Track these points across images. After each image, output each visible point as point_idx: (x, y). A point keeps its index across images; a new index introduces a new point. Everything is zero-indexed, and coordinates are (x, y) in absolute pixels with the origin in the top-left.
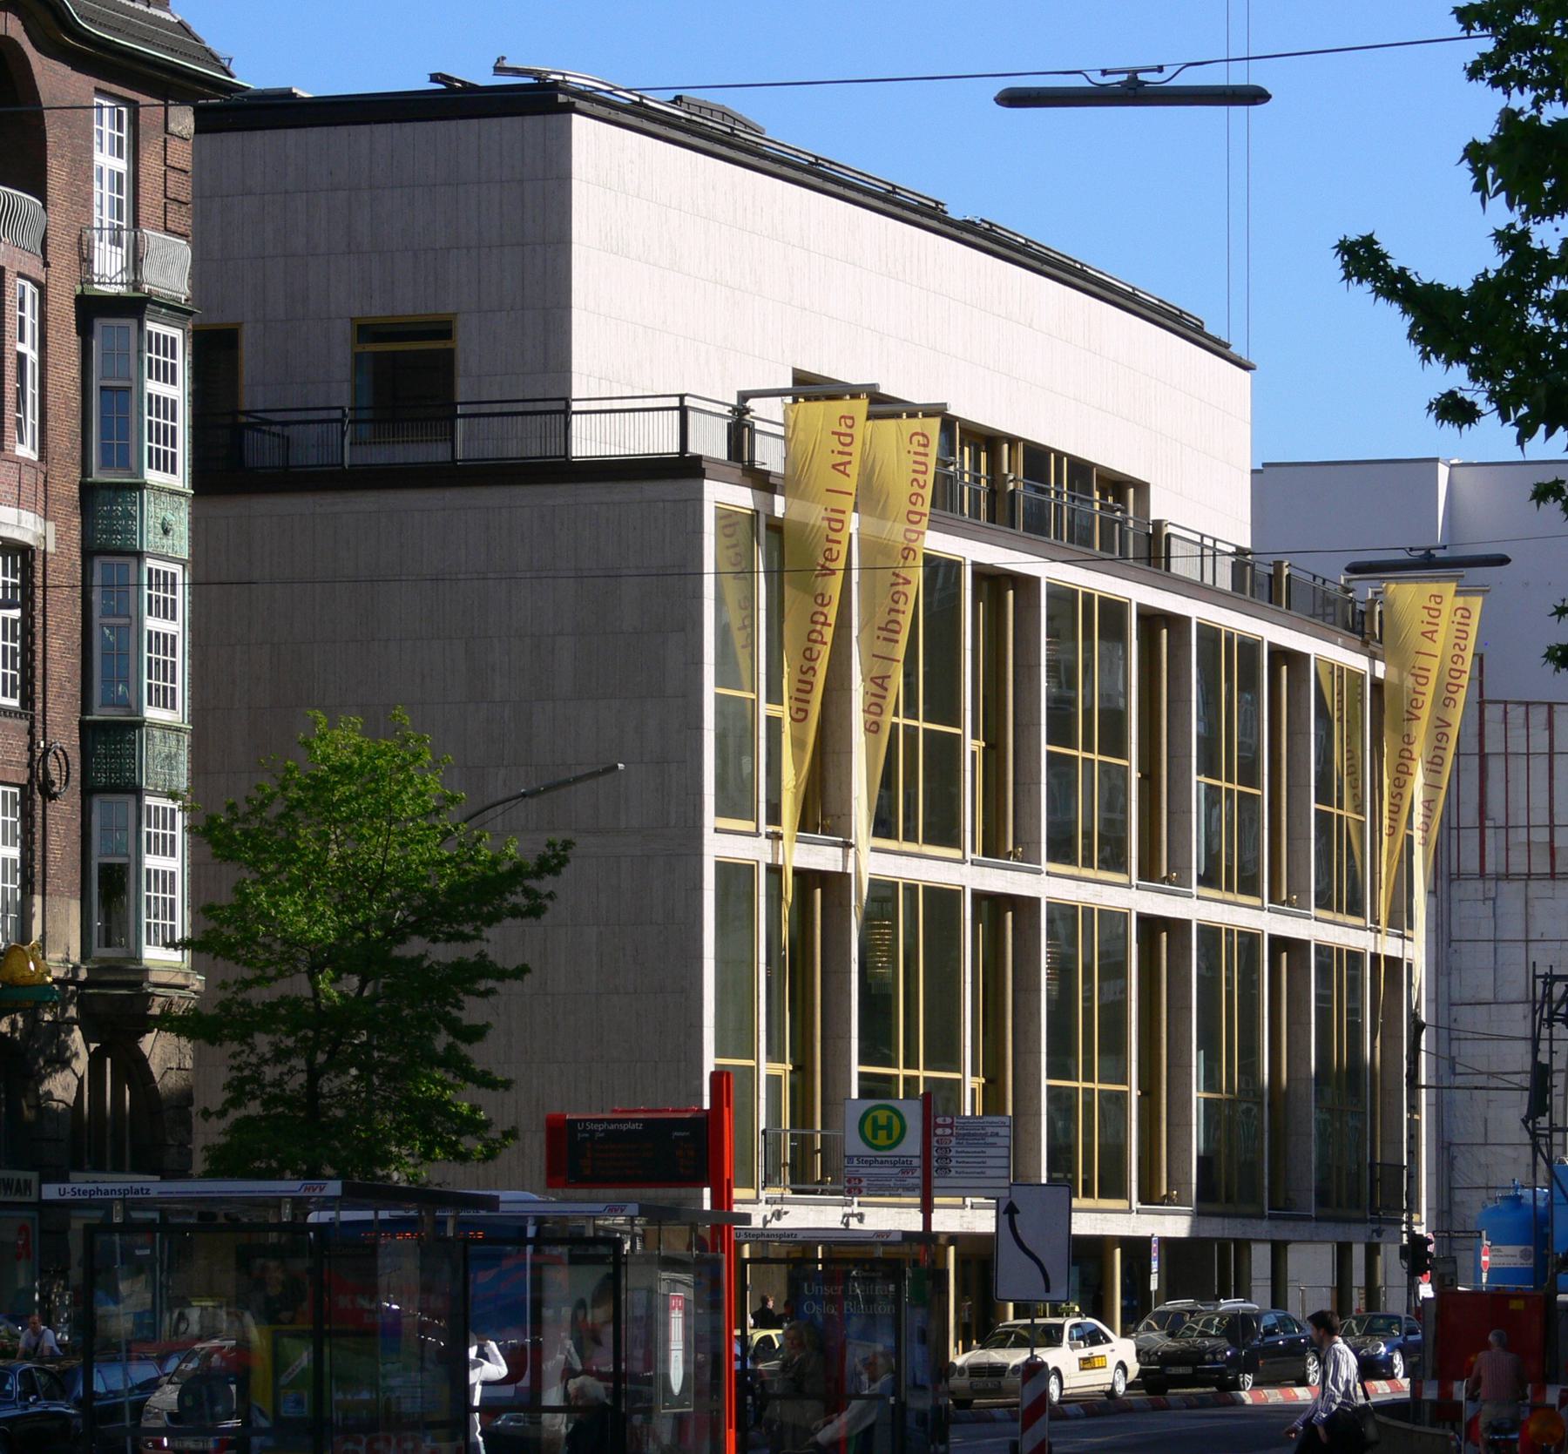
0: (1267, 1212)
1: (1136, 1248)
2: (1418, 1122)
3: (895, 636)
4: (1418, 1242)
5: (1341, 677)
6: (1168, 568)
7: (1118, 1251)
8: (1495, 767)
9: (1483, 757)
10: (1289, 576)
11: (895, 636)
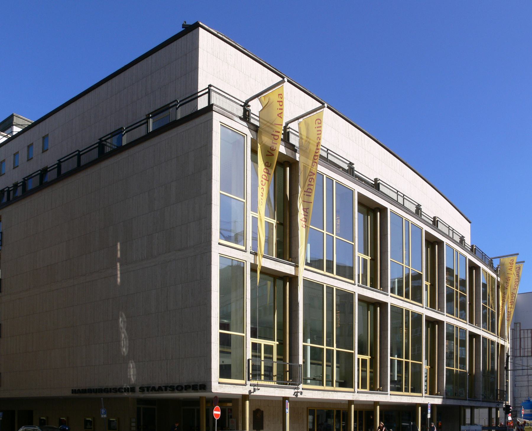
1: (424, 407)
3: (311, 194)
4: (508, 407)
5: (489, 277)
7: (420, 408)
8: (522, 340)
9: (520, 338)
11: (311, 194)
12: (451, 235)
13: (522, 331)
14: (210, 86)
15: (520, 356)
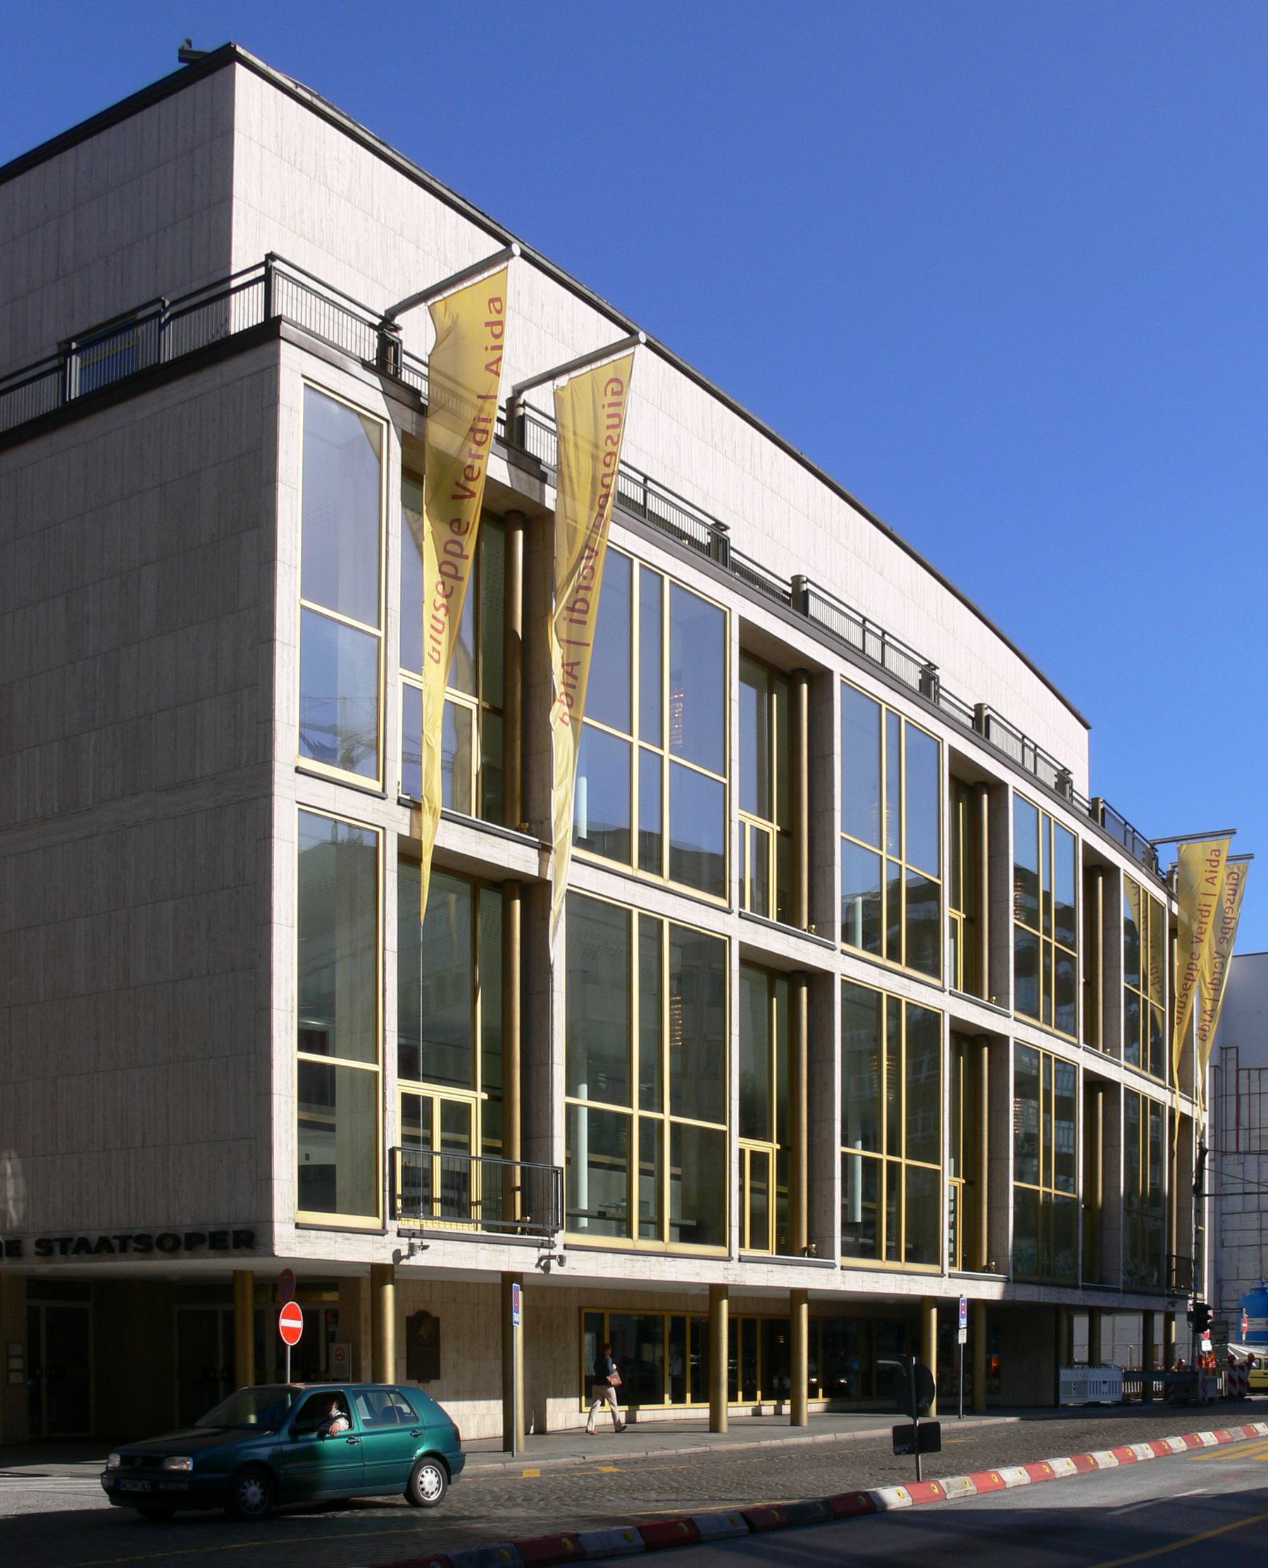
0: (1080, 1283)
1: (948, 1308)
2: (1203, 1232)
6: (988, 736)
7: (934, 1311)
8: (1244, 1100)
9: (1238, 1096)
10: (1103, 810)
12: (1029, 765)
13: (1243, 1074)
14: (271, 257)
15: (1238, 1152)
